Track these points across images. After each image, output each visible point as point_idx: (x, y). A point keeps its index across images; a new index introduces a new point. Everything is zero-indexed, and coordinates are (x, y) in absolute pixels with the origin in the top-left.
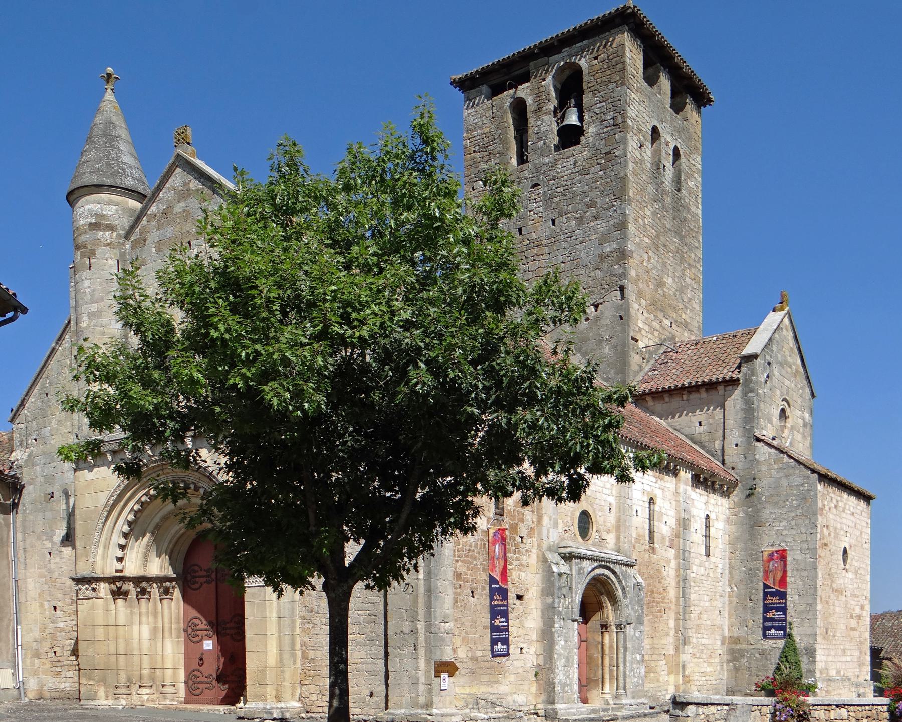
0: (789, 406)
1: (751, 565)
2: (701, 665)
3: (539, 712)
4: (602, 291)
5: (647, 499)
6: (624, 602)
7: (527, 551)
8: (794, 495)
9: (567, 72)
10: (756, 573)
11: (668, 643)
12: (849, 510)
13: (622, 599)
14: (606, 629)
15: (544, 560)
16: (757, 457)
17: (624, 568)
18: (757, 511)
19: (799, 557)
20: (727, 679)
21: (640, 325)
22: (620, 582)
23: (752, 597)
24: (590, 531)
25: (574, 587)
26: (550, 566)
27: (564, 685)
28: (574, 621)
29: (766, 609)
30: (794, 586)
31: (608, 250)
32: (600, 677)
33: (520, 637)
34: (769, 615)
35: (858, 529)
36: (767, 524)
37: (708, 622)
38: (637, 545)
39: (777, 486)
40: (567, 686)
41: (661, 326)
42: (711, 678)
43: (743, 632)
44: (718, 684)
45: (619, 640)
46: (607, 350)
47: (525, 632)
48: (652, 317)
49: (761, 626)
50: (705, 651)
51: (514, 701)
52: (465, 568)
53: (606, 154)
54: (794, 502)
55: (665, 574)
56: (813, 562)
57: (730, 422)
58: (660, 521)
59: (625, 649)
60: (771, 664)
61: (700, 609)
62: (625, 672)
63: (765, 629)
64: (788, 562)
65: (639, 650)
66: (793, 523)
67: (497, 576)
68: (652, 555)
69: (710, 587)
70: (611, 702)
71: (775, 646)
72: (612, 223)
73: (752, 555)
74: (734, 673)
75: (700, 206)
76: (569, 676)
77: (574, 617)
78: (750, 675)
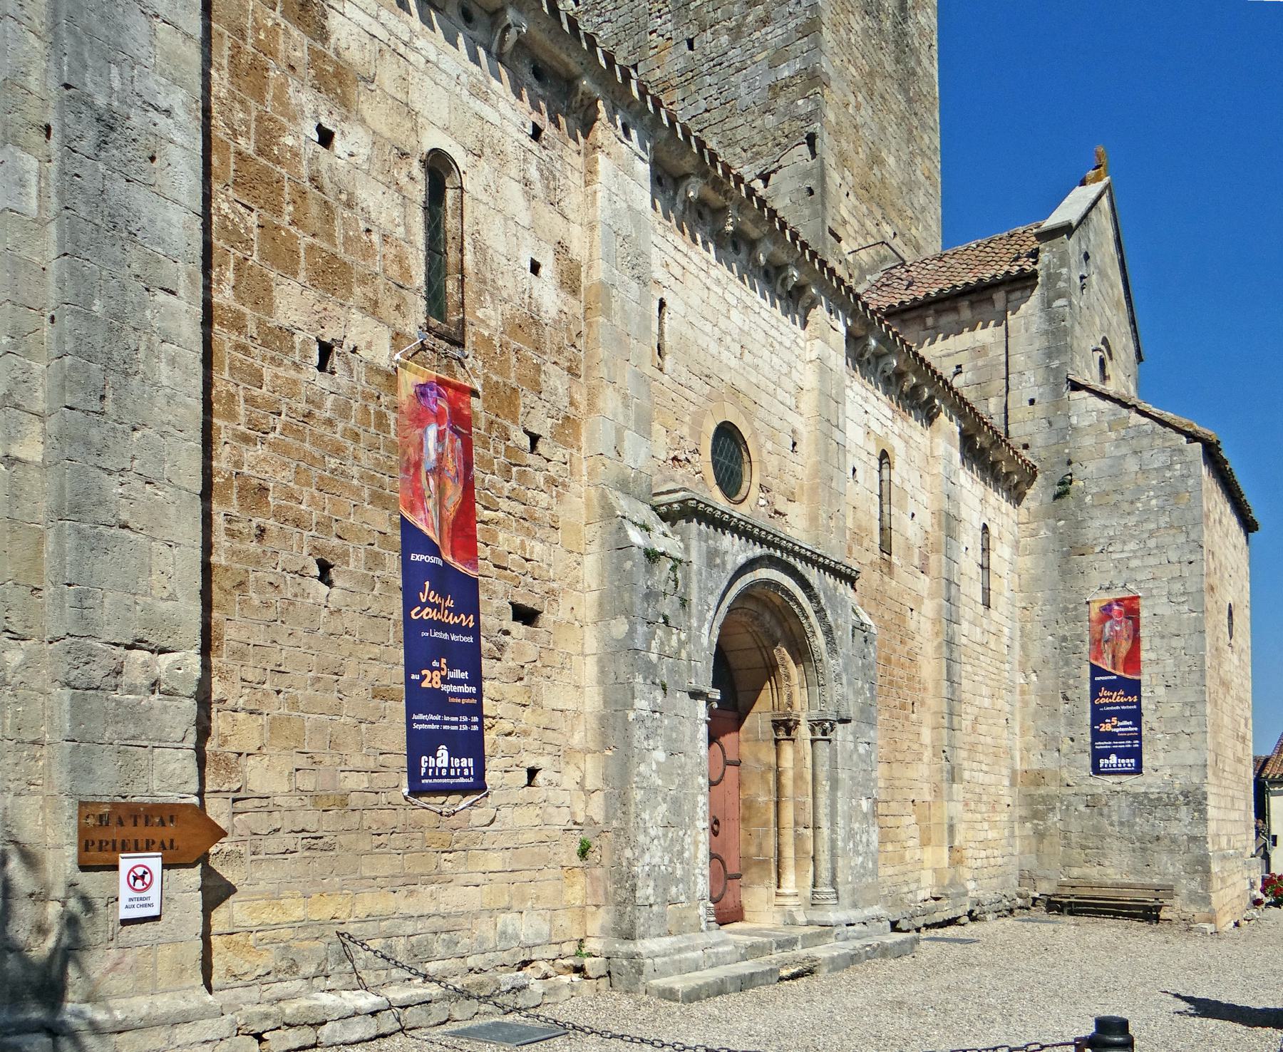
0: (1111, 358)
1: (1065, 630)
2: (978, 826)
3: (588, 962)
4: (777, 149)
6: (832, 665)
7: (551, 482)
8: (1153, 488)
10: (1077, 646)
11: (923, 771)
13: (825, 656)
14: (788, 733)
15: (608, 512)
16: (1074, 420)
17: (830, 580)
18: (1078, 525)
19: (1165, 610)
20: (1022, 853)
22: (820, 612)
23: (1069, 694)
24: (745, 484)
25: (694, 600)
26: (621, 528)
27: (665, 881)
28: (696, 695)
29: (1099, 715)
30: (1156, 669)
31: (786, 74)
32: (772, 852)
33: (526, 733)
34: (1106, 727)
36: (1097, 549)
37: (989, 740)
38: (856, 548)
39: (1116, 474)
40: (677, 882)
41: (879, 231)
42: (996, 853)
43: (1051, 762)
44: (1006, 864)
45: (819, 761)
47: (544, 721)
48: (864, 208)
49: (1089, 749)
50: (985, 798)
51: (503, 934)
54: (1154, 502)
55: (912, 625)
56: (1196, 618)
57: (1018, 360)
58: (902, 508)
59: (835, 783)
60: (1112, 824)
61: (976, 711)
62: (833, 842)
63: (1097, 755)
64: (1143, 622)
65: (865, 786)
66: (1152, 543)
67: (427, 524)
69: (991, 669)
70: (801, 918)
71: (1119, 789)
72: (791, 25)
73: (1069, 613)
74: (1034, 841)
75: (936, 65)
76: (681, 852)
77: (694, 684)
78: (1068, 845)
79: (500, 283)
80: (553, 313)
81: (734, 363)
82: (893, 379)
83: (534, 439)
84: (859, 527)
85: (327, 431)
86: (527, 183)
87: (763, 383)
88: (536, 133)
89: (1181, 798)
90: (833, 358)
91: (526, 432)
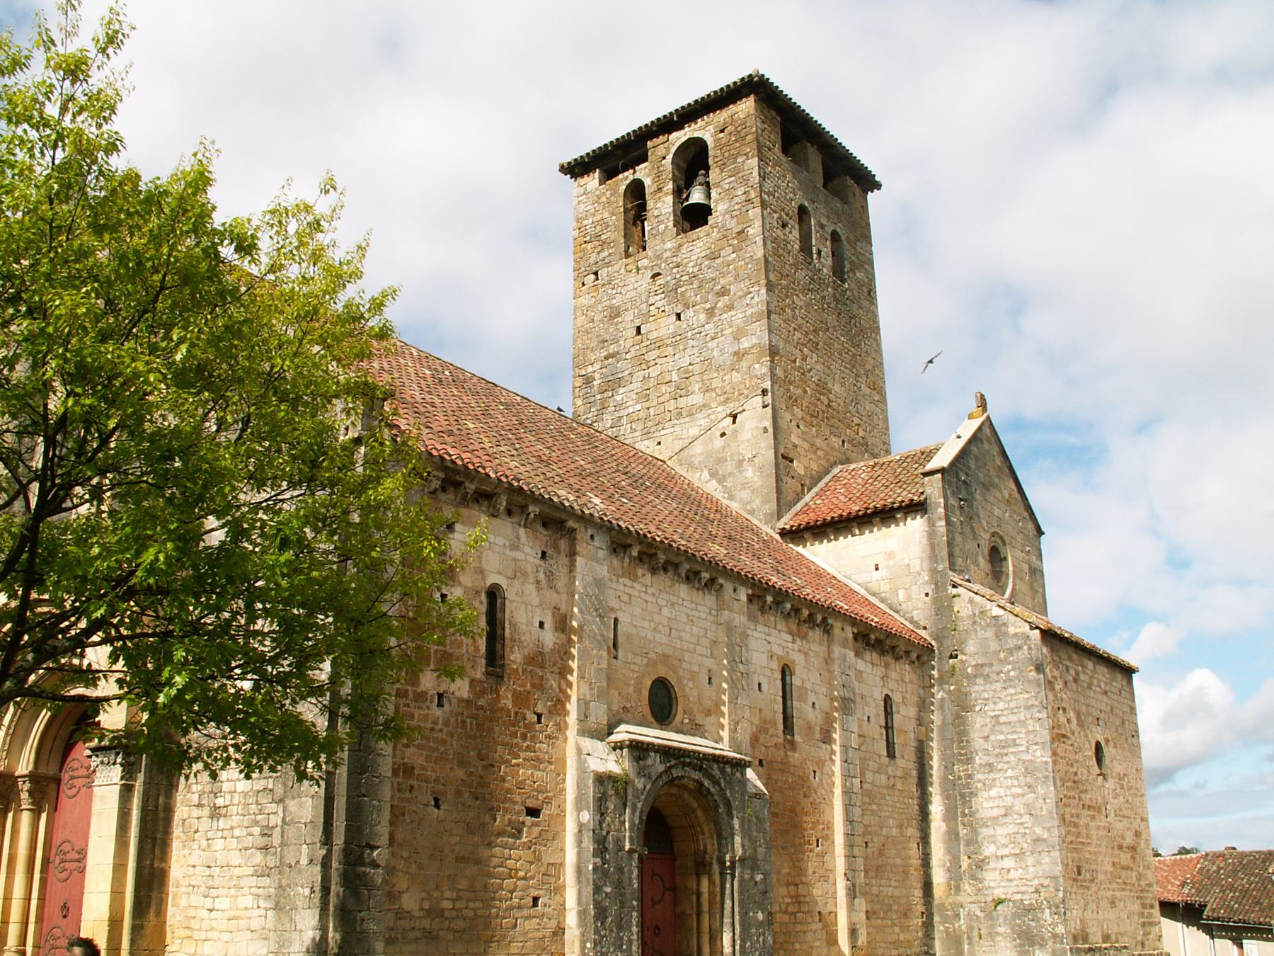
5: (776, 666)
9: (693, 150)
12: (1100, 687)
21: (794, 439)
35: (1116, 716)
37: (898, 861)
46: (749, 473)
52: (423, 758)
53: (739, 233)
54: (1012, 673)
58: (800, 699)
68: (789, 753)
72: (748, 313)
79: (523, 639)
80: (551, 646)
81: (665, 640)
82: (793, 614)
83: (539, 716)
84: (765, 722)
85: (440, 735)
86: (538, 582)
87: (685, 646)
88: (544, 555)
89: (1045, 903)
90: (737, 619)
91: (535, 713)
